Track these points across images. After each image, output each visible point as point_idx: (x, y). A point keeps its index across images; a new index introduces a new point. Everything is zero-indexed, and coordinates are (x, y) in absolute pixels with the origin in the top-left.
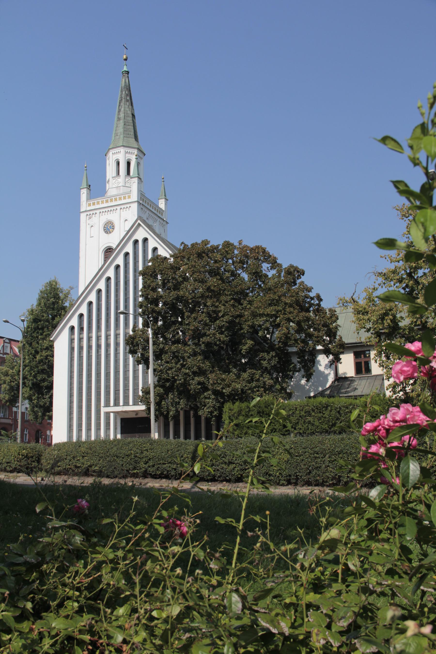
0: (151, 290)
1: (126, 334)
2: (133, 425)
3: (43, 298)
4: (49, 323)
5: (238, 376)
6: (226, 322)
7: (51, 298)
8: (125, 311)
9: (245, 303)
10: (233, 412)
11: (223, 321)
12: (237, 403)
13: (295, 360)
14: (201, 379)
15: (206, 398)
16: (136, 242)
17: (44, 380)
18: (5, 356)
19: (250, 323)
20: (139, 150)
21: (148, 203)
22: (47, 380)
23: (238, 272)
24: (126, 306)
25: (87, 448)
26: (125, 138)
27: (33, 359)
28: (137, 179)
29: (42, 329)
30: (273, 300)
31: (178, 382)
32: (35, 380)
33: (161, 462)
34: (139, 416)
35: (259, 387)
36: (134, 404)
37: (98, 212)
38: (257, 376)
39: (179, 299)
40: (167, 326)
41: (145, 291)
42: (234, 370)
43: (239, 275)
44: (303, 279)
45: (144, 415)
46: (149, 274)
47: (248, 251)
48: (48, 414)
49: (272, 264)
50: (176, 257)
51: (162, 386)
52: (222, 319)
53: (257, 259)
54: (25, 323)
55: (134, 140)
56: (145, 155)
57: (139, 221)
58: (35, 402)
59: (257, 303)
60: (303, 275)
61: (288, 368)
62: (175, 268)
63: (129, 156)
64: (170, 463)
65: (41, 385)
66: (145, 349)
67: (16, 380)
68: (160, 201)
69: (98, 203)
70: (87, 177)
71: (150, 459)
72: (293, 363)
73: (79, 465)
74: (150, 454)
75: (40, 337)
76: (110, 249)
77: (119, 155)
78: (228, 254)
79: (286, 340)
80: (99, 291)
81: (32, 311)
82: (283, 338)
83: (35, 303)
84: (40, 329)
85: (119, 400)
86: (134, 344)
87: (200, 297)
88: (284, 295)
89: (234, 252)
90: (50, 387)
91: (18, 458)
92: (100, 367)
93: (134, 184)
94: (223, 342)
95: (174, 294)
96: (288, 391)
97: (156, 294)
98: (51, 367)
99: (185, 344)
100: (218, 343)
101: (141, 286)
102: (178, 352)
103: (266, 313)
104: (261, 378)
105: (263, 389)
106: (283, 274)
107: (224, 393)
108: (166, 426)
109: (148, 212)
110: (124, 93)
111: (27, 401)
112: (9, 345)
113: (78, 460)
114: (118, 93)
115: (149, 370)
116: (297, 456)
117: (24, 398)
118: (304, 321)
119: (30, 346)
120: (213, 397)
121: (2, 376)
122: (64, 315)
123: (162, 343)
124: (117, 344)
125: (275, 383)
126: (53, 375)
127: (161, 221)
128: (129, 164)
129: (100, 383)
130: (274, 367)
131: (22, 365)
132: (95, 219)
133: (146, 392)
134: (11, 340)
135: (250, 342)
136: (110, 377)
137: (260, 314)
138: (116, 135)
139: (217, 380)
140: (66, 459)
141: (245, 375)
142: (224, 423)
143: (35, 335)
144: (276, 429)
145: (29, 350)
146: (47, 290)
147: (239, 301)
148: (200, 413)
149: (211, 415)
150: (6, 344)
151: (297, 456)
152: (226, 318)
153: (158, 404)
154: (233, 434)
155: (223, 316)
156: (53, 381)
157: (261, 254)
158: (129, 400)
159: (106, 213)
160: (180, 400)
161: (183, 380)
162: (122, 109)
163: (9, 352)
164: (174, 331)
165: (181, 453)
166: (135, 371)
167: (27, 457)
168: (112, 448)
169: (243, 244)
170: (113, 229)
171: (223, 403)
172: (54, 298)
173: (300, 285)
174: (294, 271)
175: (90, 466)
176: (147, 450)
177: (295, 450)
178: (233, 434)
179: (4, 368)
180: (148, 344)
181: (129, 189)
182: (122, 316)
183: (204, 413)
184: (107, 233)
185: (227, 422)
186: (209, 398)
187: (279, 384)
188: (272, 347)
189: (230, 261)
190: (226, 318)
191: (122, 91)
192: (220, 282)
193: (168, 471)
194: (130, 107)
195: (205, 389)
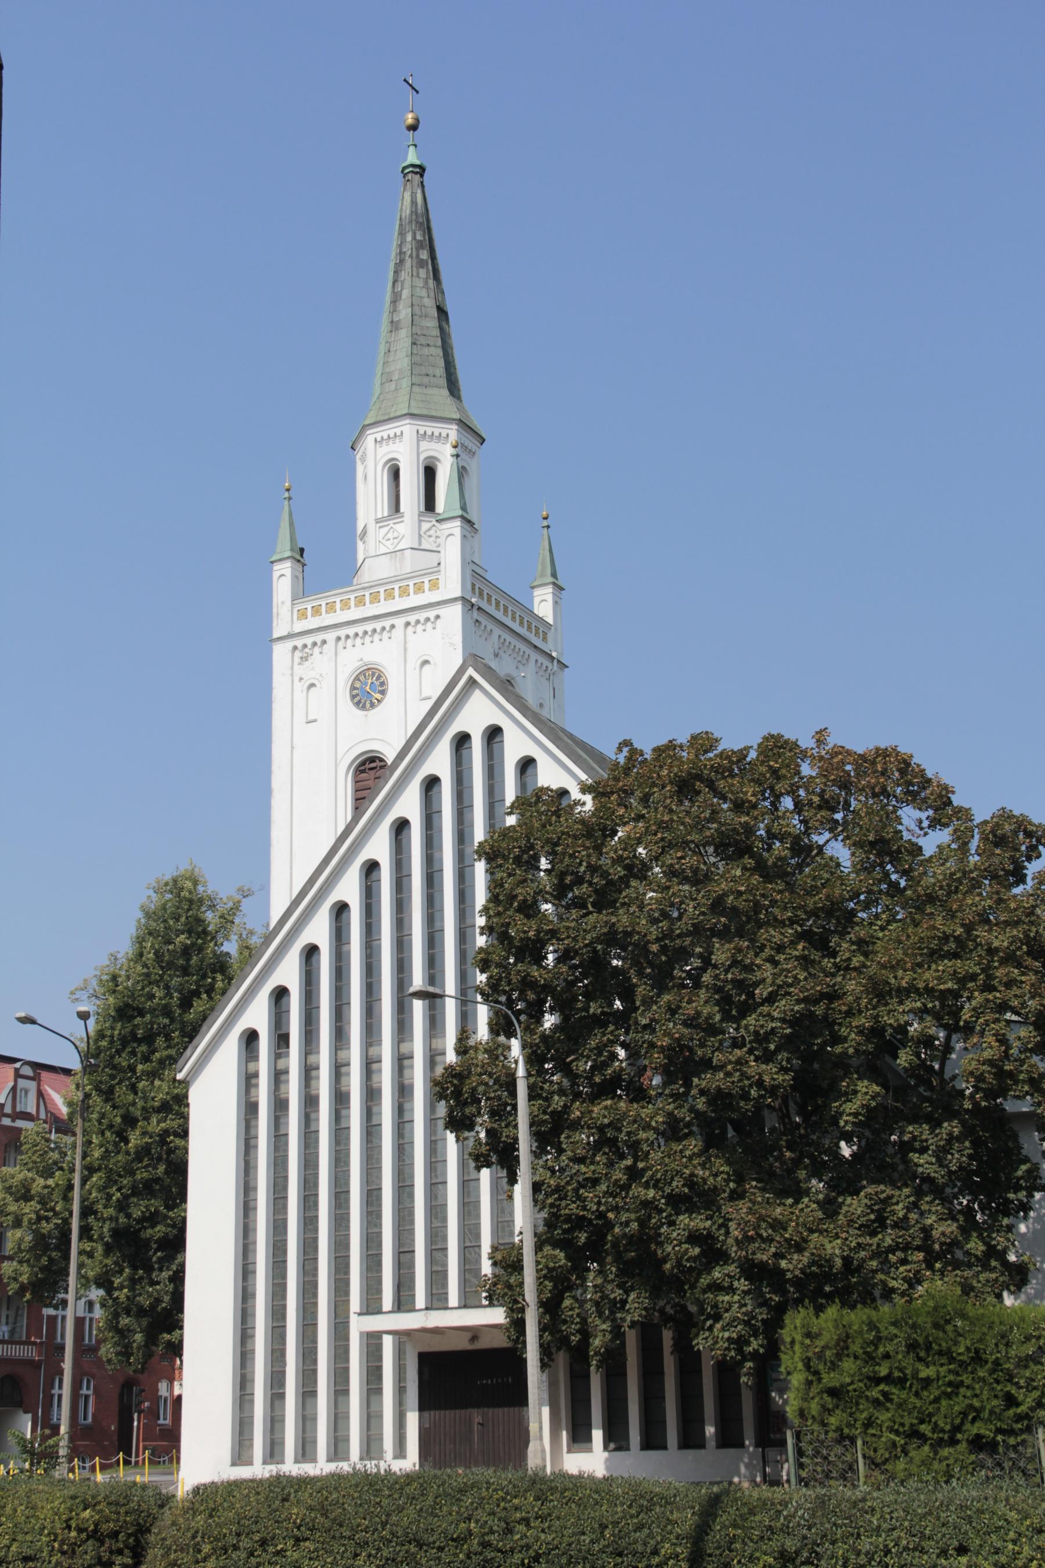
0: (519, 910)
1: (433, 1056)
2: (461, 1382)
3: (150, 934)
4: (172, 1020)
5: (830, 1208)
6: (783, 1020)
7: (179, 933)
8: (431, 989)
10: (820, 1343)
11: (773, 1019)
12: (832, 1312)
14: (699, 1222)
16: (462, 740)
17: (152, 1219)
18: (20, 1123)
19: (862, 1021)
20: (464, 425)
21: (498, 603)
22: (166, 1217)
23: (815, 838)
24: (433, 962)
25: (311, 1509)
26: (416, 389)
28: (458, 523)
29: (149, 1039)
30: (946, 938)
31: (617, 1230)
32: (122, 1220)
34: (485, 1343)
35: (906, 1247)
36: (464, 1305)
37: (330, 636)
38: (900, 1210)
39: (612, 938)
40: (573, 1032)
42: (817, 1185)
43: (820, 848)
45: (501, 1341)
46: (506, 854)
47: (848, 768)
48: (166, 1336)
50: (604, 794)
51: (565, 1244)
52: (765, 1009)
54: (91, 1022)
57: (471, 672)
58: (122, 1295)
59: (927, 1041)
61: (1009, 1178)
62: (597, 830)
63: (429, 449)
66: (503, 1112)
67: (56, 1214)
68: (537, 592)
69: (331, 608)
70: (291, 524)
72: (1026, 1160)
75: (140, 1067)
76: (372, 760)
77: (397, 445)
78: (778, 778)
79: (1001, 1078)
80: (341, 909)
81: (114, 978)
84: (140, 1041)
85: (412, 1287)
86: (464, 1096)
89: (798, 773)
90: (176, 1243)
91: (62, 1542)
93: (450, 541)
94: (773, 1091)
96: (1012, 1258)
98: (179, 1170)
99: (639, 1094)
101: (481, 897)
102: (615, 1125)
103: (921, 985)
104: (913, 1216)
105: (921, 1256)
106: (974, 843)
107: (783, 1272)
109: (497, 631)
110: (409, 238)
112: (32, 1085)
113: (278, 1553)
114: (390, 241)
115: (517, 1188)
117: (85, 1282)
119: (106, 1101)
120: (742, 1285)
121: (9, 1199)
123: (562, 1092)
124: (403, 1091)
126: (183, 1198)
127: (542, 659)
128: (430, 473)
129: (348, 1228)
130: (963, 1178)
131: (78, 1167)
132: (321, 663)
133: (509, 1262)
134: (37, 1066)
136: (380, 1205)
137: (899, 990)
139: (757, 1227)
140: (236, 1547)
141: (854, 1206)
142: (786, 1382)
143: (123, 1061)
144: (978, 1411)
145: (103, 1116)
146: (164, 908)
147: (821, 943)
148: (700, 1343)
149: (740, 1351)
150: (22, 1083)
152: (783, 1006)
153: (550, 1307)
154: (824, 1424)
155: (771, 999)
156: (184, 1220)
158: (445, 1285)
159: (358, 641)
160: (627, 1292)
161: (635, 1225)
162: (406, 294)
163: (31, 1109)
164: (599, 1050)
165: (650, 1535)
166: (467, 1187)
167: (96, 1535)
168: (400, 1510)
169: (832, 741)
170: (383, 693)
172: (190, 932)
174: (1015, 832)
176: (526, 1521)
178: (824, 1424)
179: (16, 1172)
180: (513, 1094)
181: (432, 559)
182: (418, 1007)
183: (712, 1342)
184: (360, 713)
186: (731, 1290)
187: (980, 1237)
189: (787, 803)
190: (783, 1006)
191: (402, 234)
192: (756, 879)
194: (431, 283)
195: (713, 1254)
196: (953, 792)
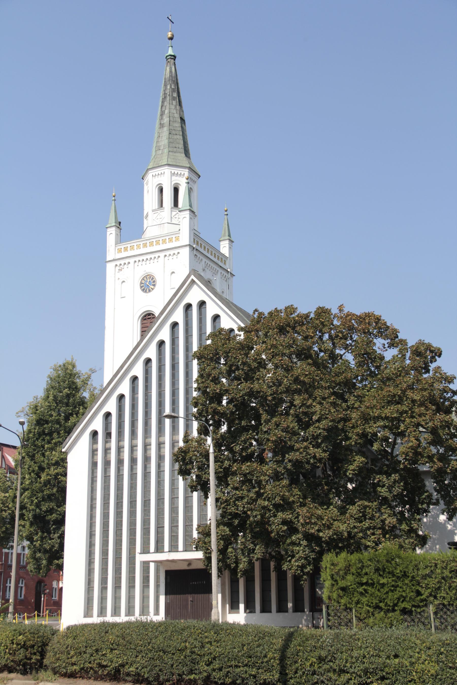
0: (212, 381)
1: (174, 443)
2: (184, 583)
4: (61, 426)
5: (343, 510)
6: (324, 429)
7: (65, 388)
8: (173, 414)
9: (352, 400)
11: (320, 428)
12: (343, 555)
13: (430, 484)
14: (287, 516)
15: (293, 544)
16: (188, 307)
17: (51, 511)
19: (359, 430)
20: (191, 169)
21: (205, 247)
22: (57, 511)
24: (174, 402)
25: (118, 636)
26: (171, 153)
27: (36, 479)
28: (188, 212)
29: (50, 434)
30: (394, 396)
32: (38, 510)
33: (233, 663)
34: (193, 567)
35: (374, 528)
36: (185, 550)
37: (132, 260)
39: (252, 394)
40: (233, 435)
41: (203, 382)
43: (341, 356)
44: (439, 362)
45: (201, 566)
46: (207, 357)
48: (56, 561)
49: (392, 340)
50: (248, 332)
51: (229, 525)
52: (317, 425)
53: (367, 333)
55: (183, 155)
56: (199, 177)
57: (192, 277)
58: (38, 544)
60: (439, 356)
62: (246, 347)
63: (176, 180)
64: (246, 665)
65: (47, 518)
66: (204, 468)
68: (222, 243)
69: (132, 248)
71: (214, 658)
72: (427, 491)
73: (105, 663)
74: (216, 649)
75: (46, 446)
76: (149, 314)
79: (416, 454)
82: (411, 454)
83: (41, 394)
84: (46, 435)
85: (163, 542)
86: (186, 461)
87: (284, 392)
88: (411, 387)
90: (61, 522)
92: (136, 493)
93: (184, 219)
94: (320, 460)
95: (244, 387)
97: (219, 386)
98: (63, 491)
100: (312, 461)
101: (195, 375)
103: (383, 415)
106: (408, 355)
107: (321, 538)
108: (234, 583)
109: (204, 260)
110: (169, 87)
111: (26, 543)
113: (103, 655)
114: (161, 89)
116: (450, 668)
117: (21, 538)
118: (443, 427)
119: (32, 460)
120: (304, 543)
122: (83, 414)
123: (229, 459)
124: (160, 458)
125: (400, 522)
127: (224, 272)
128: (176, 190)
129: (135, 516)
130: (399, 497)
131: (19, 488)
133: (205, 532)
135: (359, 460)
138: (158, 148)
140: (85, 652)
141: (353, 510)
143: (39, 443)
144: (405, 597)
145: (30, 466)
149: (302, 571)
151: (450, 668)
152: (324, 424)
153: (222, 552)
154: (338, 602)
155: (319, 421)
156: (65, 512)
157: (373, 325)
160: (255, 545)
161: (259, 517)
162: (167, 111)
164: (245, 441)
165: (264, 649)
166: (188, 500)
167: (24, 646)
170: (154, 285)
171: (321, 554)
172: (69, 388)
173: (436, 372)
174: (426, 350)
175: (123, 665)
176: (210, 643)
177: (446, 657)
178: (338, 602)
180: (208, 460)
182: (167, 422)
183: (292, 567)
184: (144, 293)
185: (327, 584)
186: (299, 545)
188: (392, 466)
190: (324, 424)
191: (165, 85)
192: (313, 369)
193: (243, 679)
194: (178, 107)
195: (293, 530)
196: (399, 332)
